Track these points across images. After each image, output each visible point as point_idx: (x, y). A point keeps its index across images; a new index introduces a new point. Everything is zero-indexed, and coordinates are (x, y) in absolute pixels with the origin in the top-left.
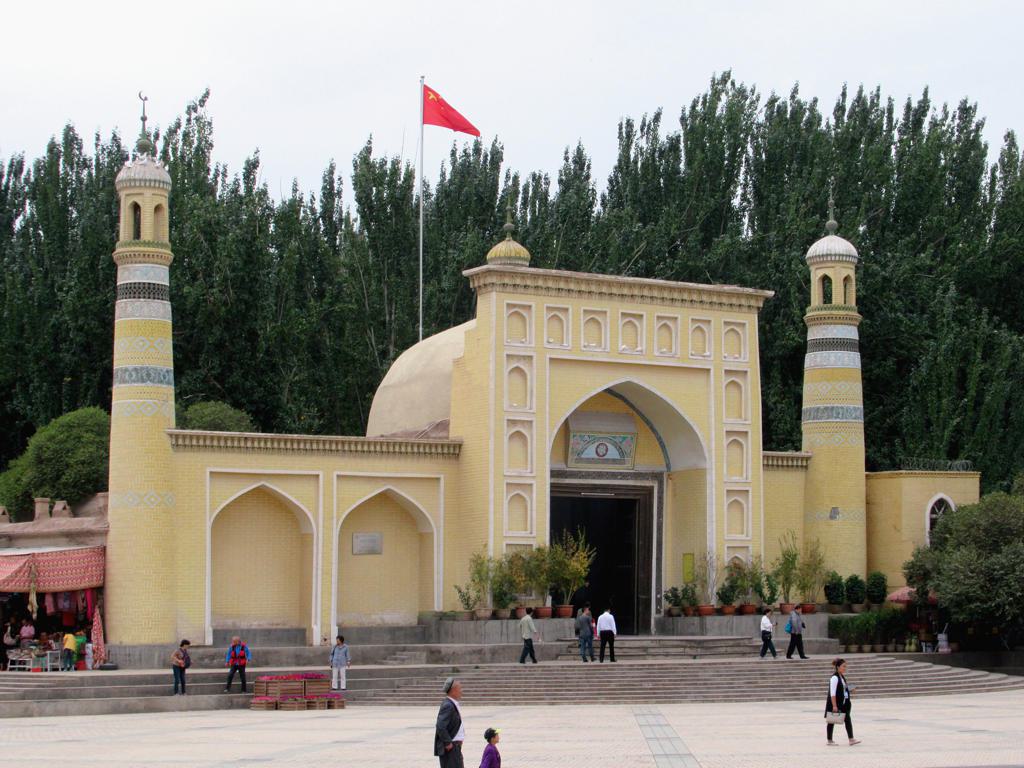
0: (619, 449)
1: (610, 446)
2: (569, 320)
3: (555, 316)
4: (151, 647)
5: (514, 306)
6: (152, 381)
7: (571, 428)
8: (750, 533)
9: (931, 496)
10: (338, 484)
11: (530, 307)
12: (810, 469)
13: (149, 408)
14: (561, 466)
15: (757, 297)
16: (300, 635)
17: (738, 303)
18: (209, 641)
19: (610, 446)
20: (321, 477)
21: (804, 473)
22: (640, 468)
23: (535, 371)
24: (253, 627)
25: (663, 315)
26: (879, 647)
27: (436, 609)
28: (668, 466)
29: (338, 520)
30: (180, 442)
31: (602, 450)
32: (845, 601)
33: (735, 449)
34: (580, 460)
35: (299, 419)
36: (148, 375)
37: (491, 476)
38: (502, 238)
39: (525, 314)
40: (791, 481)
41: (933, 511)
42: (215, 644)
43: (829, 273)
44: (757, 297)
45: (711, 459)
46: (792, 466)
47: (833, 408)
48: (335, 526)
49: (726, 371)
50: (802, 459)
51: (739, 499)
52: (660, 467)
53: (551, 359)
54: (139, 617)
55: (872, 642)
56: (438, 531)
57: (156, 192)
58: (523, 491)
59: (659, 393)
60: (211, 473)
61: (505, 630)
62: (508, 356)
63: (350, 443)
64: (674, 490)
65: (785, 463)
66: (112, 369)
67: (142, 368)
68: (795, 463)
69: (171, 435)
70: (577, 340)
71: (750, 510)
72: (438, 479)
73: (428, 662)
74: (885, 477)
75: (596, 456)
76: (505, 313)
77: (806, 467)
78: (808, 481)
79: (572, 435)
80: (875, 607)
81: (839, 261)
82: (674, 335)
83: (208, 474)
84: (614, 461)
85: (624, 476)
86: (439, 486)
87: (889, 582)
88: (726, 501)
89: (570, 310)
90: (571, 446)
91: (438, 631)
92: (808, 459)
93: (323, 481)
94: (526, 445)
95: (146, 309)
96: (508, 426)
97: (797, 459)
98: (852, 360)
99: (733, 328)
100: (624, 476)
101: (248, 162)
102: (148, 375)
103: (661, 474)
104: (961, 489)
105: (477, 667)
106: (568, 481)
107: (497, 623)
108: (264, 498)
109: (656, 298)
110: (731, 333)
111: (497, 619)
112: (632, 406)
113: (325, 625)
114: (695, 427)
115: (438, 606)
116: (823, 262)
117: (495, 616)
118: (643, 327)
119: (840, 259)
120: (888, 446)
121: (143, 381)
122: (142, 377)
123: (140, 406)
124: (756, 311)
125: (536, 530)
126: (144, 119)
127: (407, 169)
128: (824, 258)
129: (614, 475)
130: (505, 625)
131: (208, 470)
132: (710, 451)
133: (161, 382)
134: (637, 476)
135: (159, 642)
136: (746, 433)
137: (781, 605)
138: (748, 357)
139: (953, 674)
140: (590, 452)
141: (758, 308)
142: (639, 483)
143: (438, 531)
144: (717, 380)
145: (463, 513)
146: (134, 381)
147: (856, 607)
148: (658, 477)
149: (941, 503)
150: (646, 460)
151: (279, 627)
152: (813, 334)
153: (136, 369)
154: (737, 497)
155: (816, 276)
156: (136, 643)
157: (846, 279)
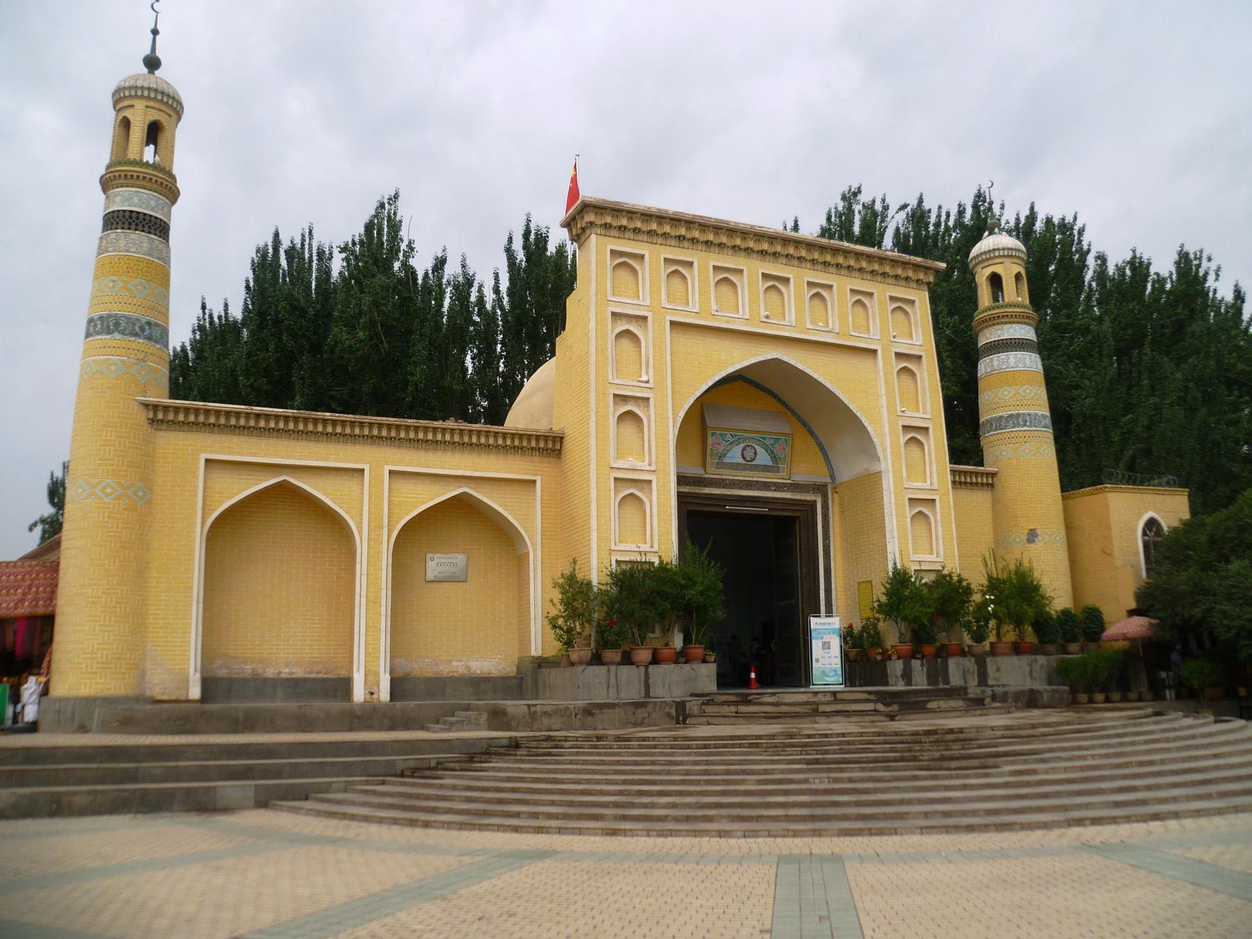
0: (772, 454)
1: (759, 449)
2: (693, 276)
3: (676, 272)
4: (90, 702)
5: (622, 254)
6: (122, 332)
7: (709, 424)
8: (942, 553)
9: (1140, 516)
11: (642, 257)
12: (998, 486)
13: (113, 368)
14: (695, 471)
15: (927, 269)
16: (344, 686)
18: (195, 692)
19: (759, 449)
21: (989, 494)
22: (799, 478)
23: (651, 334)
24: (283, 676)
26: (1116, 696)
27: (533, 653)
28: (832, 476)
30: (160, 416)
31: (749, 454)
32: (1061, 641)
33: (914, 448)
34: (721, 465)
36: (117, 325)
37: (593, 466)
40: (979, 500)
41: (1144, 534)
42: (205, 698)
43: (998, 269)
44: (927, 269)
45: (885, 457)
47: (1018, 415)
49: (897, 354)
50: (988, 474)
51: (924, 510)
52: (822, 478)
53: (672, 323)
55: (1105, 689)
56: (535, 551)
57: (152, 104)
58: (641, 491)
59: (816, 376)
60: (207, 461)
61: (613, 681)
62: (614, 314)
63: (407, 428)
64: (841, 505)
67: (109, 316)
71: (939, 524)
72: (534, 482)
73: (490, 728)
74: (1084, 495)
75: (741, 460)
76: (609, 262)
77: (992, 485)
78: (995, 502)
79: (710, 432)
80: (1092, 646)
81: (1008, 256)
82: (829, 306)
83: (202, 463)
84: (766, 468)
85: (779, 487)
86: (534, 491)
87: (1106, 617)
88: (908, 513)
89: (695, 264)
90: (709, 447)
91: (536, 681)
92: (994, 475)
94: (642, 431)
95: (122, 243)
96: (615, 403)
97: (982, 474)
98: (1031, 362)
99: (901, 306)
100: (779, 487)
101: (437, 259)
102: (117, 325)
103: (825, 486)
104: (1170, 507)
106: (707, 491)
107: (600, 670)
108: (285, 500)
111: (603, 664)
112: (784, 404)
113: (371, 675)
114: (864, 420)
115: (536, 650)
116: (990, 258)
117: (597, 660)
118: (790, 292)
119: (1009, 254)
120: (1082, 464)
121: (109, 333)
122: (108, 327)
124: (926, 288)
125: (657, 538)
126: (155, 32)
128: (990, 255)
129: (766, 486)
130: (612, 673)
132: (884, 450)
133: (136, 335)
134: (795, 487)
135: (106, 693)
136: (927, 429)
137: (991, 644)
138: (919, 334)
139: (1181, 729)
140: (735, 456)
141: (928, 284)
142: (798, 496)
143: (535, 551)
144: (885, 365)
145: (566, 523)
146: (98, 333)
147: (1073, 647)
148: (821, 489)
149: (1152, 523)
150: (806, 470)
151: (320, 676)
152: (987, 337)
153: (101, 318)
154: (921, 506)
155: (982, 276)
156: (74, 693)
157: (1018, 277)
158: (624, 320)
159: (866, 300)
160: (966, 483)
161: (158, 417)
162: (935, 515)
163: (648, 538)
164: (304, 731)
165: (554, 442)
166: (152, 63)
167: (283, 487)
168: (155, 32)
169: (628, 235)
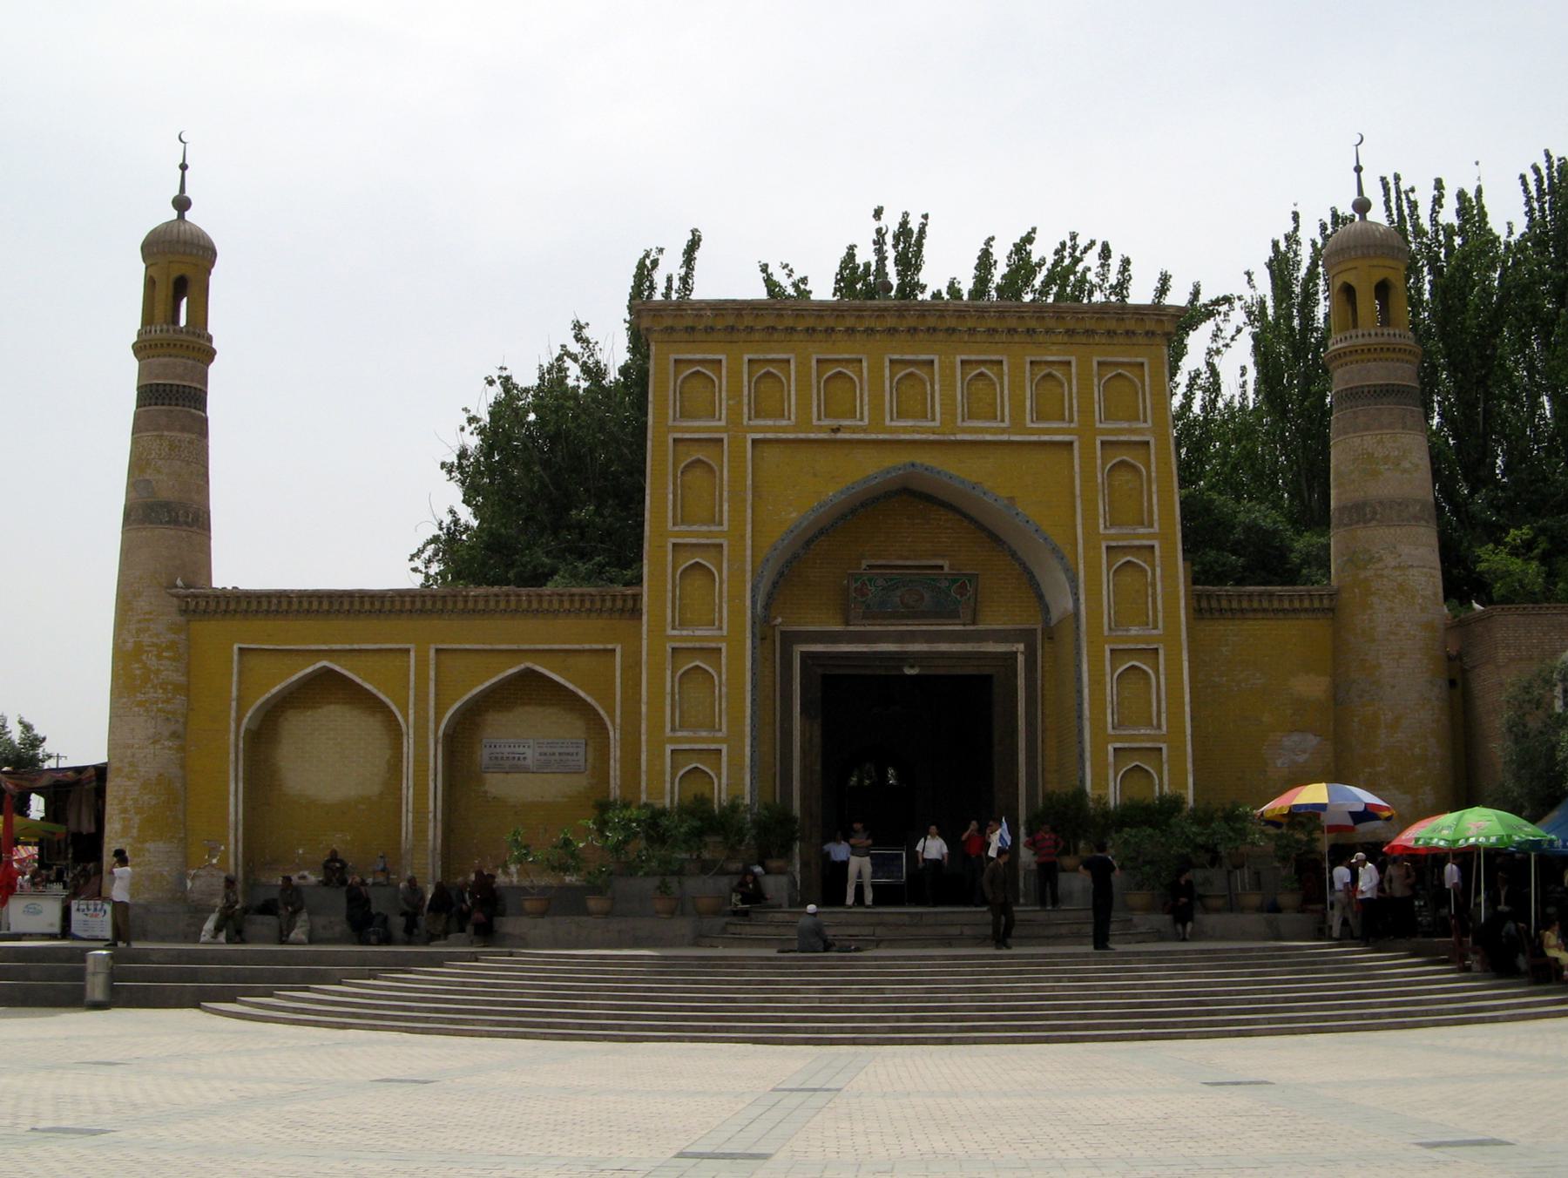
126: (184, 167)
131: (236, 647)
148: (1027, 636)
167: (529, 674)
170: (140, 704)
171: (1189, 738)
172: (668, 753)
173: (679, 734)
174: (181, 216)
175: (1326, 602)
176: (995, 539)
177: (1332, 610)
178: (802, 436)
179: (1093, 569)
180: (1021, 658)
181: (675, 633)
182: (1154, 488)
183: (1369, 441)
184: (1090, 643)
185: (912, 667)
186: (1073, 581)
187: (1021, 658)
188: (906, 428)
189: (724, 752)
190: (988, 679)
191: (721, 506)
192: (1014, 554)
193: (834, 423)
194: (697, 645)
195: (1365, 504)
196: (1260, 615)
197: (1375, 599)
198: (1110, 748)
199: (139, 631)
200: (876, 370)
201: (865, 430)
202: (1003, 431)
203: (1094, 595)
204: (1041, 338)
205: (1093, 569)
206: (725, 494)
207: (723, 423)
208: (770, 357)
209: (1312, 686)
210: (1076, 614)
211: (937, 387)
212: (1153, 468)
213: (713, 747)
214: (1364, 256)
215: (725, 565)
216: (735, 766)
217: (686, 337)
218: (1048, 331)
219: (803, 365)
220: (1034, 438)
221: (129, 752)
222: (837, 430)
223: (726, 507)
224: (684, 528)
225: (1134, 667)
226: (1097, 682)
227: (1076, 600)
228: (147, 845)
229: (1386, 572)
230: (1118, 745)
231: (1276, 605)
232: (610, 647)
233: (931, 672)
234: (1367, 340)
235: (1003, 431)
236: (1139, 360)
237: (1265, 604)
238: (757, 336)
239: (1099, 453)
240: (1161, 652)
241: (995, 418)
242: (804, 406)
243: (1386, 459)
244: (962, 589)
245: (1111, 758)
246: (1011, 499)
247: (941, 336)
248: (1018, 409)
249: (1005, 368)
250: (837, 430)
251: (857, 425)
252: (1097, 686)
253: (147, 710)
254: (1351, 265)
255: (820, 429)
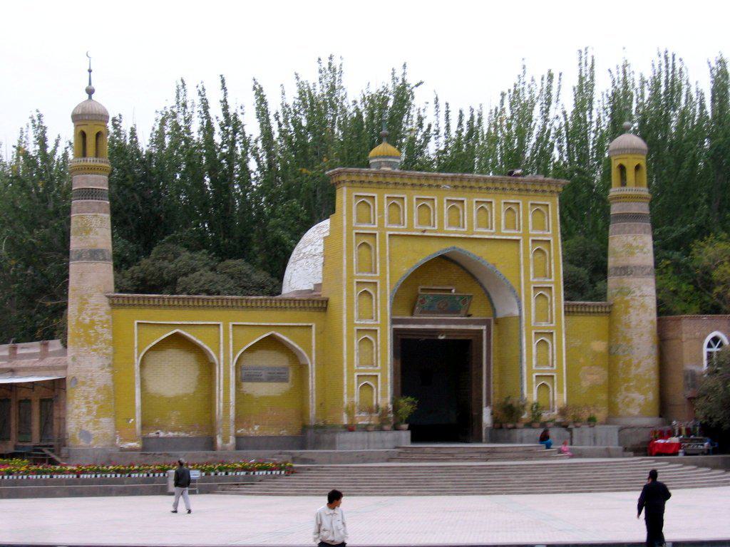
10: (138, 329)
12: (329, 308)
17: (419, 183)
20: (379, 332)
25: (536, 202)
29: (233, 359)
35: (224, 290)
38: (380, 142)
39: (369, 202)
40: (590, 324)
43: (624, 162)
46: (594, 312)
48: (136, 360)
54: (86, 424)
65: (596, 310)
66: (606, 266)
68: (320, 305)
69: (109, 297)
70: (412, 222)
86: (311, 331)
92: (611, 306)
93: (226, 331)
99: (539, 210)
103: (489, 320)
105: (280, 454)
109: (466, 187)
110: (538, 213)
119: (634, 151)
123: (90, 283)
126: (90, 71)
127: (697, 92)
128: (622, 151)
131: (136, 322)
144: (526, 251)
148: (487, 322)
154: (544, 338)
157: (638, 168)
158: (363, 237)
159: (514, 208)
160: (589, 312)
161: (114, 304)
162: (552, 341)
163: (517, 226)
164: (522, 378)
165: (323, 303)
166: (90, 92)
167: (176, 335)
168: (90, 71)
169: (365, 185)
170: (95, 350)
171: (564, 372)
172: (356, 376)
173: (360, 368)
174: (90, 97)
175: (607, 310)
176: (474, 277)
177: (610, 312)
178: (409, 233)
179: (528, 296)
180: (485, 333)
181: (358, 322)
182: (552, 261)
183: (630, 239)
184: (526, 329)
185: (442, 336)
186: (519, 302)
187: (485, 333)
188: (451, 231)
189: (379, 377)
190: (470, 340)
191: (376, 265)
192: (481, 285)
193: (423, 228)
194: (367, 328)
195: (627, 267)
196: (580, 314)
197: (630, 309)
198: (534, 376)
199: (92, 314)
200: (441, 204)
201: (436, 232)
202: (492, 234)
203: (528, 311)
204: (508, 192)
205: (528, 296)
206: (378, 260)
207: (376, 226)
208: (396, 196)
209: (599, 346)
210: (520, 317)
211: (465, 213)
212: (552, 251)
213: (375, 374)
214: (631, 154)
215: (378, 292)
216: (384, 383)
217: (359, 185)
218: (512, 189)
219: (410, 201)
220: (504, 237)
221: (90, 374)
222: (424, 231)
223: (378, 265)
224: (361, 274)
225: (544, 338)
226: (529, 346)
227: (520, 310)
228: (101, 420)
229: (636, 298)
230: (537, 374)
231: (587, 310)
232: (310, 324)
233: (450, 338)
234: (630, 193)
235: (492, 234)
236: (547, 203)
237: (583, 310)
238: (391, 186)
239: (530, 245)
240: (554, 334)
241: (488, 227)
242: (410, 219)
243: (637, 247)
244: (464, 302)
245: (534, 380)
246: (494, 264)
247: (467, 190)
248: (498, 224)
249: (494, 205)
250: (424, 231)
251: (431, 230)
252: (529, 349)
253: (98, 353)
254: (625, 156)
255: (417, 230)
